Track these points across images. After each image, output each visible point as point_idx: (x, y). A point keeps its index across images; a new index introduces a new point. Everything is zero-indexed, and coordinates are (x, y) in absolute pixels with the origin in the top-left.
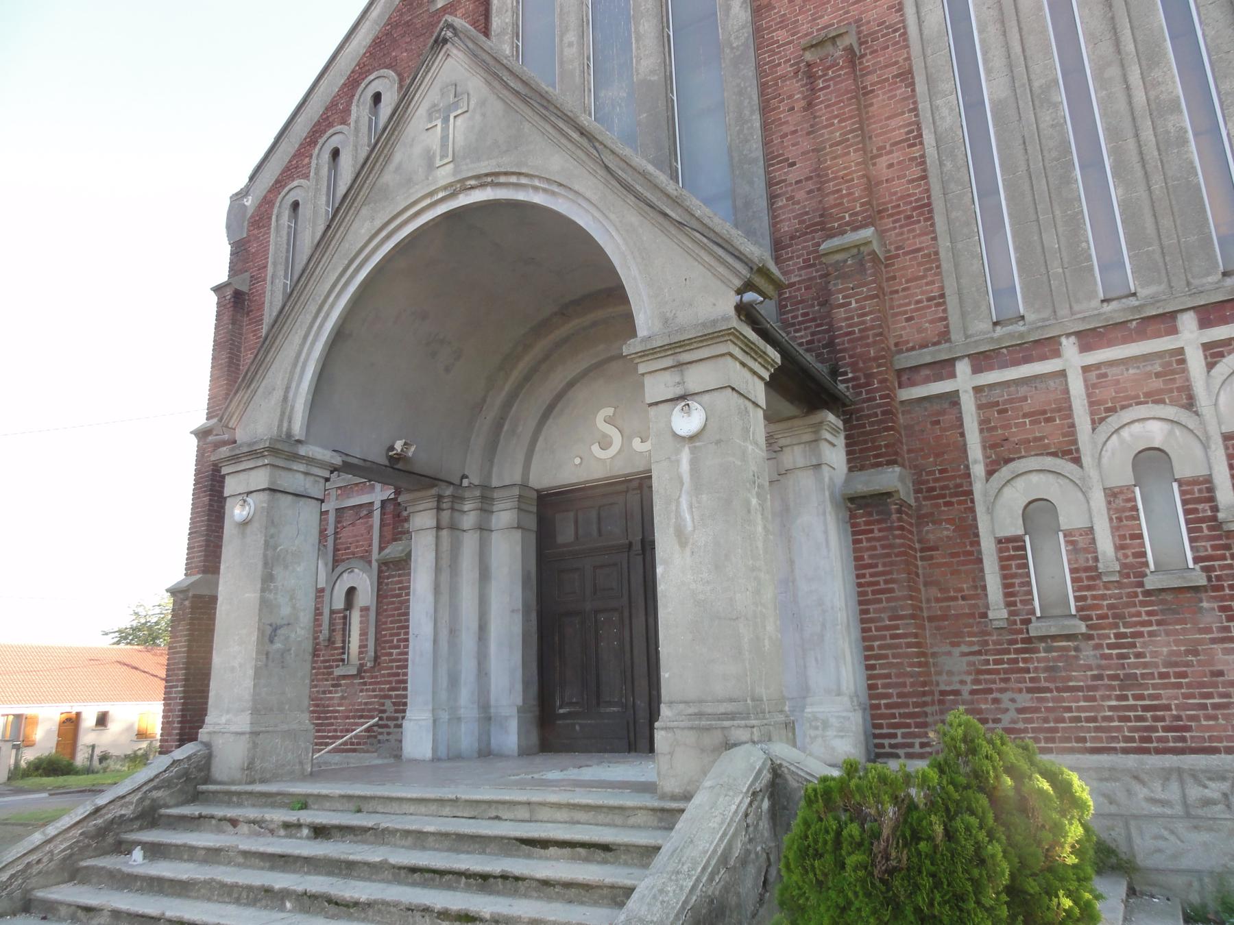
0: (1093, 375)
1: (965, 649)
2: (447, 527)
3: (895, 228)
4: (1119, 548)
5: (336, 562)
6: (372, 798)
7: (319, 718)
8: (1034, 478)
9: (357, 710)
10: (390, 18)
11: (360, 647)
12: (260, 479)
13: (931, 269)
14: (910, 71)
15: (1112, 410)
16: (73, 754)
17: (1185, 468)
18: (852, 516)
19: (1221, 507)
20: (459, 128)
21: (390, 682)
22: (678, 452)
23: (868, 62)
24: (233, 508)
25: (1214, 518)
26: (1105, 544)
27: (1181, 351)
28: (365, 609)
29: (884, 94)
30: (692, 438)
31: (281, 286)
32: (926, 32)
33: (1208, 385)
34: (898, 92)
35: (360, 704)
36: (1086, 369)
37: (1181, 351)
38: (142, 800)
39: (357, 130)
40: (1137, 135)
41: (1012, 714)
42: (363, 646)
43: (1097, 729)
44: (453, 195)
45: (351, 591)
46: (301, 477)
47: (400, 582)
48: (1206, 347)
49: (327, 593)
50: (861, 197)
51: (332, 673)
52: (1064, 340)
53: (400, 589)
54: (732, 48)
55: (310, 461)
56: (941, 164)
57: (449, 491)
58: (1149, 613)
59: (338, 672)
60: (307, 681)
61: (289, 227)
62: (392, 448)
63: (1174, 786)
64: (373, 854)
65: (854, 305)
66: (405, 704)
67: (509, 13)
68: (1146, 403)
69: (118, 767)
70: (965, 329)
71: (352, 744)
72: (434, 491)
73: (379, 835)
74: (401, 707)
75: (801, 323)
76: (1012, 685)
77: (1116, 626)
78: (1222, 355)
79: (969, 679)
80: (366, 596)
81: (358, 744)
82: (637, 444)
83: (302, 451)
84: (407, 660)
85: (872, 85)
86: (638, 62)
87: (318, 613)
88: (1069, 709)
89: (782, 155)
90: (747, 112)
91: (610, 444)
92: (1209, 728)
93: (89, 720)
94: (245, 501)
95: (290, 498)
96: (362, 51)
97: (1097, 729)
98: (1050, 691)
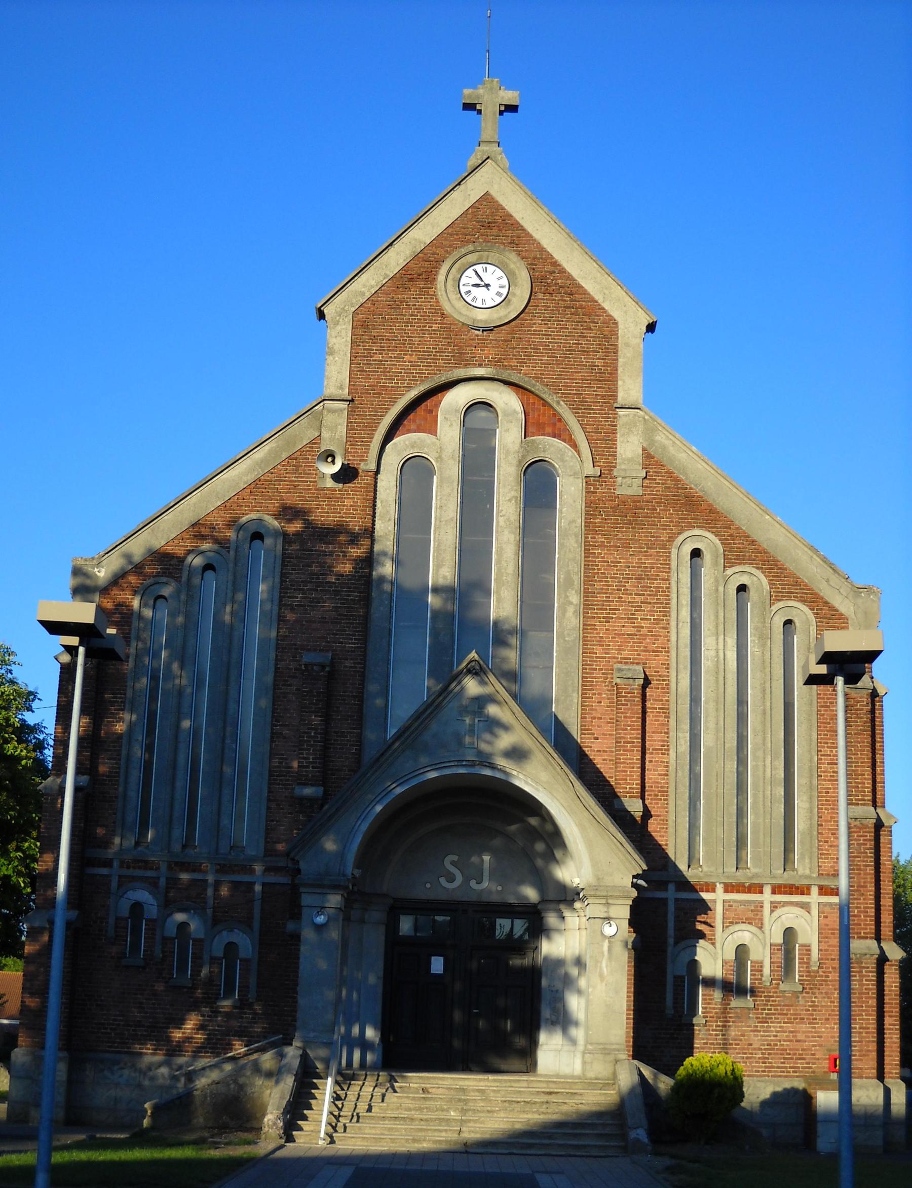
13: (663, 828)
19: (764, 975)
22: (603, 941)
25: (761, 979)
32: (679, 690)
33: (770, 921)
37: (762, 902)
40: (764, 791)
48: (772, 902)
68: (745, 923)
78: (776, 907)
82: (473, 883)
90: (570, 689)
91: (453, 881)
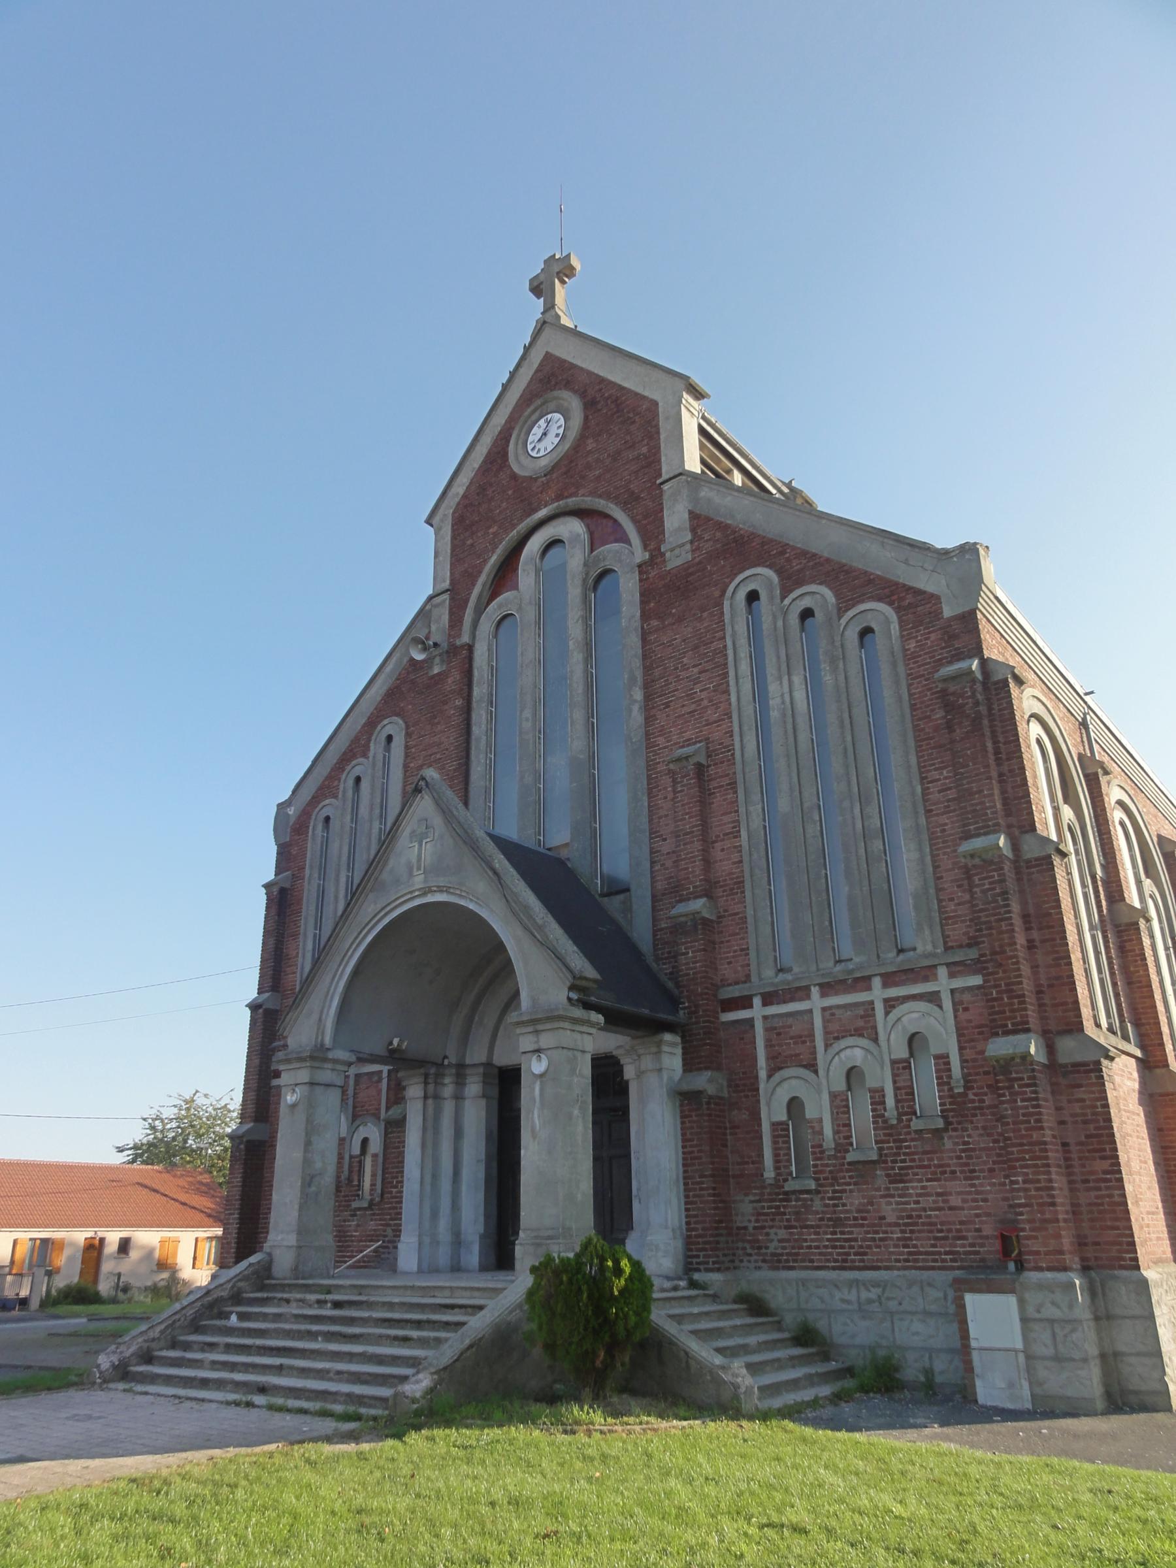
0: (827, 1013)
1: (752, 1198)
2: (432, 1097)
3: (723, 896)
4: (836, 1132)
5: (355, 1117)
6: (368, 1286)
7: (339, 1242)
8: (794, 1082)
9: (369, 1236)
10: (400, 674)
11: (371, 1185)
12: (304, 1075)
14: (735, 783)
15: (837, 1038)
16: (96, 1280)
17: (871, 1083)
18: (681, 1105)
20: (428, 851)
21: (390, 1214)
23: (712, 771)
24: (286, 1095)
26: (828, 1130)
27: (872, 1003)
28: (375, 1156)
29: (721, 796)
30: (542, 1076)
31: (315, 886)
32: (746, 755)
34: (729, 796)
35: (370, 1231)
36: (824, 1009)
38: (232, 1287)
39: (374, 765)
41: (775, 1243)
42: (373, 1185)
43: (821, 1254)
44: (424, 894)
45: (365, 1142)
46: (329, 1072)
47: (399, 1137)
48: (886, 1001)
49: (348, 1141)
50: (699, 875)
51: (350, 1205)
52: (812, 988)
53: (399, 1142)
54: (632, 743)
55: (336, 1061)
56: (750, 855)
57: (433, 1071)
58: (850, 1177)
59: (355, 1205)
60: (332, 1213)
61: (323, 836)
62: (391, 1043)
63: (854, 1291)
64: (365, 1314)
65: (690, 954)
66: (400, 1231)
67: (486, 685)
69: (142, 1298)
70: (759, 974)
71: (364, 1262)
72: (422, 1071)
73: (370, 1305)
74: (397, 1232)
75: (666, 958)
76: (777, 1223)
77: (833, 1185)
78: (893, 1007)
79: (753, 1219)
80: (376, 1146)
81: (369, 1262)
83: (330, 1055)
84: (402, 1197)
85: (714, 788)
86: (572, 742)
87: (341, 1157)
88: (806, 1240)
89: (659, 831)
92: (878, 1253)
93: (112, 1246)
94: (294, 1090)
95: (322, 1087)
96: (379, 698)
97: (821, 1254)
98: (796, 1228)
